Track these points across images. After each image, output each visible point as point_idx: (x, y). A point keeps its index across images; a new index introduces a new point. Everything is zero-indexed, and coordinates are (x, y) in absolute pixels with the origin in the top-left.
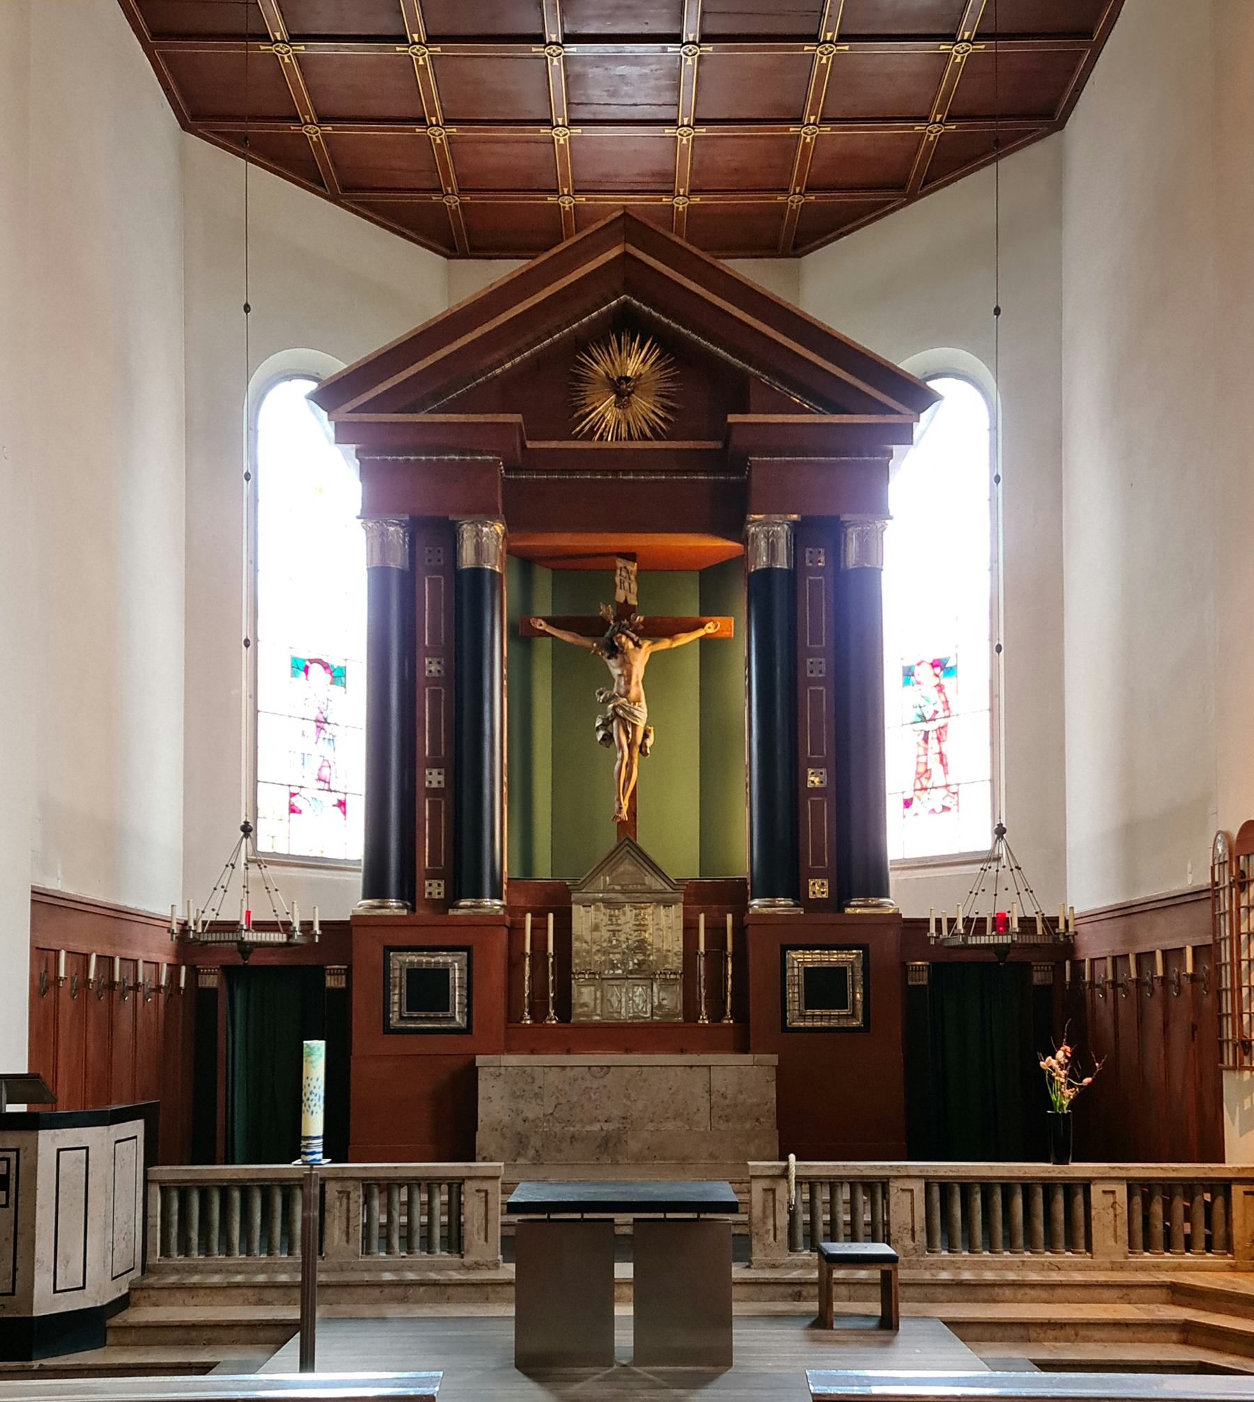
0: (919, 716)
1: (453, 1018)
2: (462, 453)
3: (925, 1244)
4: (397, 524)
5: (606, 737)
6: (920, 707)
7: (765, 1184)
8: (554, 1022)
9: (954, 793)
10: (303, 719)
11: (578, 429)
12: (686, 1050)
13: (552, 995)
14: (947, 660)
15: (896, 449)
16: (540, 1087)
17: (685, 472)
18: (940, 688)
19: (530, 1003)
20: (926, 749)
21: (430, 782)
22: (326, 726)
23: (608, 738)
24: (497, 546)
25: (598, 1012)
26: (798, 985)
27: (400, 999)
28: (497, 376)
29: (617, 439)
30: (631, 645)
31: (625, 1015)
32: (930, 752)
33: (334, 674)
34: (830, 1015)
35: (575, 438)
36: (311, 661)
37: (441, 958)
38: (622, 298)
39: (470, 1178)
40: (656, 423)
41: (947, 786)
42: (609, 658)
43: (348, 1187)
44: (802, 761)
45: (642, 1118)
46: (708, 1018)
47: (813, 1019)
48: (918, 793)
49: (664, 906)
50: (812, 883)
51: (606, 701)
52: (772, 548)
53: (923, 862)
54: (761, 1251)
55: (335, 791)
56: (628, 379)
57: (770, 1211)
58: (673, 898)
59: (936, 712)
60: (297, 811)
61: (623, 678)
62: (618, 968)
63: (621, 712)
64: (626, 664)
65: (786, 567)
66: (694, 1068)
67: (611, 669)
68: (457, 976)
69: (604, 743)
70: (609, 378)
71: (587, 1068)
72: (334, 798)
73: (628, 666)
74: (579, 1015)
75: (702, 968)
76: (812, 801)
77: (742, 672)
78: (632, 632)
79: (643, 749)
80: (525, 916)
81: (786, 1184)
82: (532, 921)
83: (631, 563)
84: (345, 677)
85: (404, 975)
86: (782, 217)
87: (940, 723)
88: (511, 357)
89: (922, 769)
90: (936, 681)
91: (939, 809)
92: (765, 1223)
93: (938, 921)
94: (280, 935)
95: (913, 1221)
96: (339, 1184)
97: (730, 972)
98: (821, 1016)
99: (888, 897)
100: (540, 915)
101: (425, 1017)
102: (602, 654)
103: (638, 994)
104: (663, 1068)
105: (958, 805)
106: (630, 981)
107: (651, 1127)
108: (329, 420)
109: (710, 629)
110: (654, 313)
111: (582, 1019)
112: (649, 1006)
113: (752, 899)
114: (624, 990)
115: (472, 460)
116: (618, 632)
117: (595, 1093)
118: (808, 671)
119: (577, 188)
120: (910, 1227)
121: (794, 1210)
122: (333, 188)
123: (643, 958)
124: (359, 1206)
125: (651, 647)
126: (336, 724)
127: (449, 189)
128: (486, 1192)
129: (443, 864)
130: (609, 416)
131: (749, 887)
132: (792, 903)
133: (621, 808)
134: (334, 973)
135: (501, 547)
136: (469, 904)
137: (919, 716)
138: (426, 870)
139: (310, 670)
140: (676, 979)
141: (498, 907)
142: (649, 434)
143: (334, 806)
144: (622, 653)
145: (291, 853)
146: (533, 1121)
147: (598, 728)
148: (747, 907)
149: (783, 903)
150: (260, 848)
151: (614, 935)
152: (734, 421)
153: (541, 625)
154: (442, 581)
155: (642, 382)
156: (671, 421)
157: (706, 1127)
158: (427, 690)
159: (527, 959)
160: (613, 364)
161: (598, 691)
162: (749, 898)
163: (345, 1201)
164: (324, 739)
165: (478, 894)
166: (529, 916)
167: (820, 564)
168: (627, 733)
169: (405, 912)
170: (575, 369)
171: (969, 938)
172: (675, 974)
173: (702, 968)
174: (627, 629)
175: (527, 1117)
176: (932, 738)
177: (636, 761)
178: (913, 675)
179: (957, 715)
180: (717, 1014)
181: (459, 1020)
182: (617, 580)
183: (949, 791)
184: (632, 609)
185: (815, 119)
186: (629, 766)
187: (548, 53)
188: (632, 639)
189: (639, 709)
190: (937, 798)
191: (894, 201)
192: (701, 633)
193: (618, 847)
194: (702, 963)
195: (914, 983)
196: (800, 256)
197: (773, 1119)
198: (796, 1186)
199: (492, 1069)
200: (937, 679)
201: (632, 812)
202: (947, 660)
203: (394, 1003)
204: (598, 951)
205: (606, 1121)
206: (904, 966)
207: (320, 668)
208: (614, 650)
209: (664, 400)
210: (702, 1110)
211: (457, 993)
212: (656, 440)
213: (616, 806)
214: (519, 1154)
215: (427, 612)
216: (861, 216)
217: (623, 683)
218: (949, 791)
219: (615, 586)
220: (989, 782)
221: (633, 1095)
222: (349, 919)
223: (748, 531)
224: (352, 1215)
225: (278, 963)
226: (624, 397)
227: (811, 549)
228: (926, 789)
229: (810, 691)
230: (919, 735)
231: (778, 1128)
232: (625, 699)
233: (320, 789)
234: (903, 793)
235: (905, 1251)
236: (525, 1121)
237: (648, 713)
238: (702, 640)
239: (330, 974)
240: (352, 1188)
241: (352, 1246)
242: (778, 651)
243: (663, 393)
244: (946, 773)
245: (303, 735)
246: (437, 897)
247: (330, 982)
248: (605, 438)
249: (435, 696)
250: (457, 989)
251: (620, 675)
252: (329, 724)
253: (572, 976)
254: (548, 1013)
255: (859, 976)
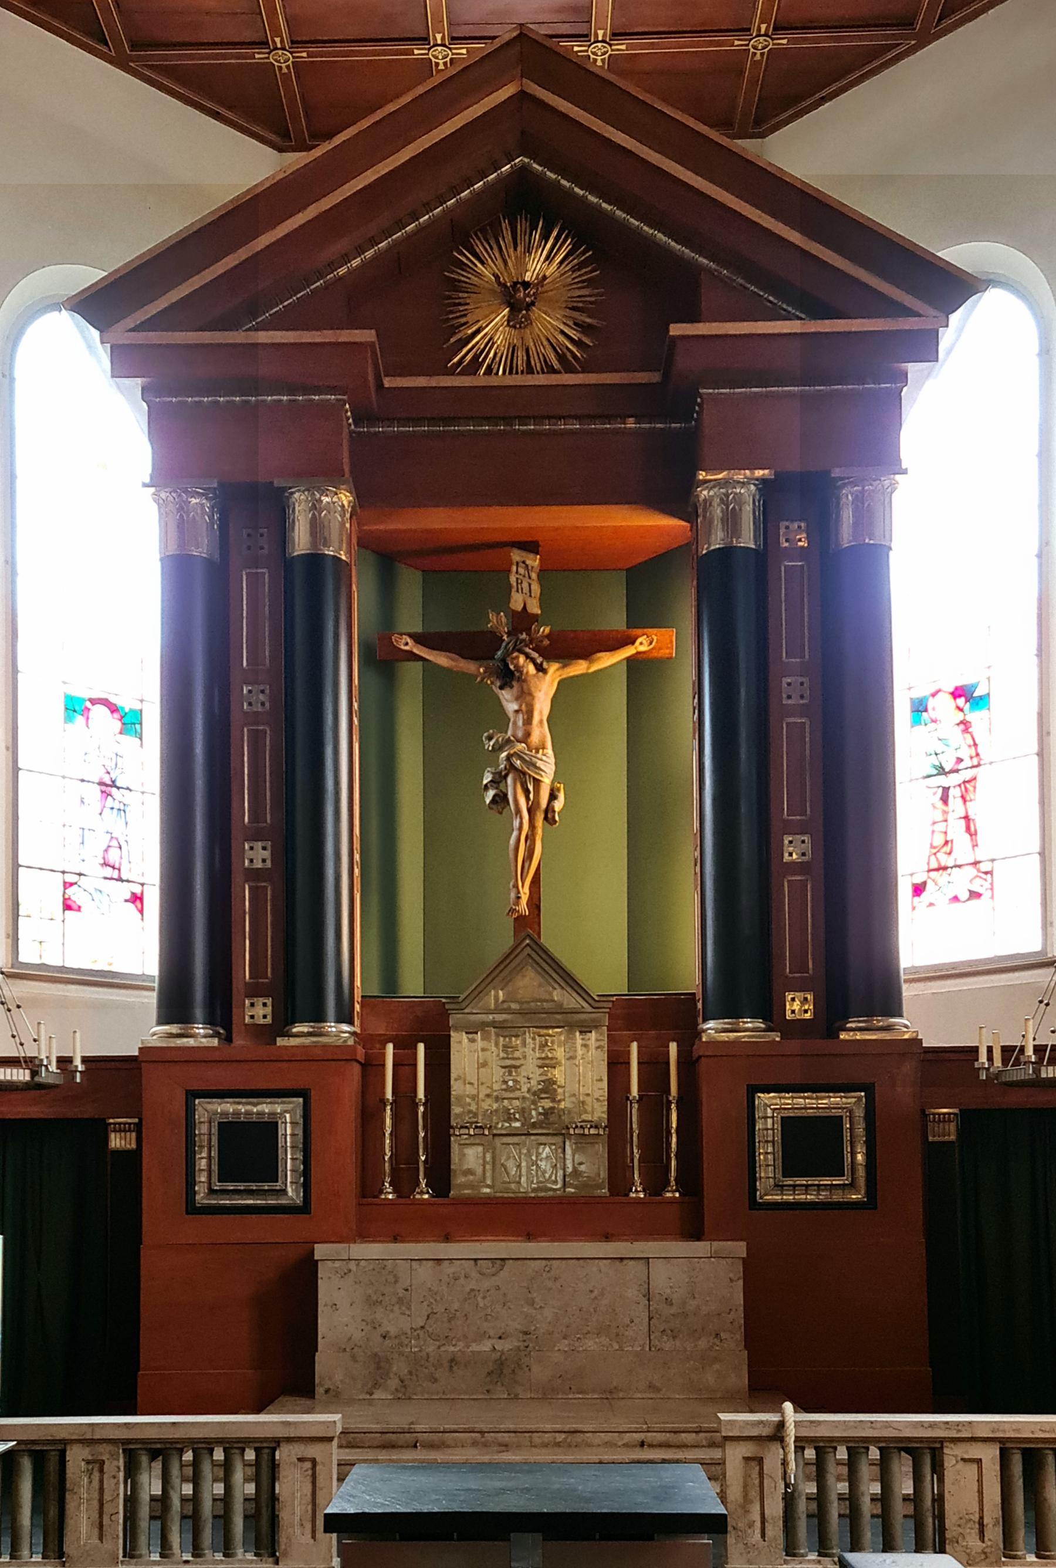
0: (935, 767)
1: (284, 1191)
2: (292, 390)
3: (1002, 1546)
4: (203, 494)
5: (497, 798)
6: (936, 754)
7: (746, 1449)
8: (426, 1196)
9: (986, 873)
10: (83, 781)
11: (455, 360)
12: (613, 1235)
13: (423, 1158)
14: (974, 687)
15: (913, 369)
16: (407, 1290)
17: (608, 418)
18: (965, 725)
19: (392, 1169)
20: (945, 813)
21: (251, 861)
22: (114, 790)
23: (501, 799)
24: (343, 524)
25: (489, 1182)
26: (773, 1142)
27: (209, 1165)
28: (341, 278)
29: (511, 373)
30: (531, 669)
31: (526, 1186)
32: (951, 817)
33: (125, 720)
34: (818, 1186)
35: (451, 372)
36: (93, 701)
37: (265, 1107)
38: (517, 161)
39: (289, 1440)
40: (567, 348)
41: (976, 863)
42: (501, 688)
43: (101, 1454)
44: (775, 826)
45: (551, 1333)
46: (644, 1190)
47: (794, 1191)
48: (933, 874)
49: (581, 1032)
50: (790, 997)
51: (498, 748)
52: (731, 521)
53: (941, 970)
54: (741, 1554)
55: (128, 881)
56: (526, 285)
57: (754, 1494)
58: (593, 1020)
59: (960, 760)
60: (74, 906)
61: (521, 716)
62: (517, 1120)
63: (518, 762)
64: (525, 697)
65: (753, 547)
66: (625, 1262)
67: (504, 703)
68: (289, 1132)
69: (494, 807)
70: (499, 283)
71: (472, 1262)
72: (126, 890)
73: (528, 698)
74: (461, 1185)
75: (634, 1119)
76: (789, 881)
77: (688, 701)
78: (533, 649)
79: (549, 816)
80: (384, 1048)
81: (781, 1451)
82: (394, 1053)
83: (532, 556)
84: (141, 724)
85: (215, 1130)
86: (741, 72)
87: (967, 775)
88: (360, 250)
89: (939, 840)
90: (960, 716)
91: (964, 895)
92: (747, 1512)
93: (990, 1050)
94: (21, 1071)
95: (981, 1510)
96: (88, 1449)
97: (674, 1125)
98: (807, 1186)
99: (901, 1016)
100: (407, 1046)
101: (245, 1190)
102: (492, 683)
103: (544, 1155)
104: (581, 1261)
105: (992, 889)
106: (533, 1138)
107: (564, 1345)
108: (102, 342)
109: (642, 645)
110: (564, 182)
111: (466, 1191)
112: (560, 1173)
113: (705, 1020)
114: (524, 1151)
115: (306, 400)
116: (514, 650)
117: (484, 1298)
118: (784, 696)
119: (454, 35)
120: (976, 1517)
121: (792, 1493)
122: (118, 45)
123: (551, 1105)
124: (118, 1483)
125: (558, 673)
126: (128, 789)
127: (278, 40)
128: (314, 1462)
129: (269, 974)
130: (499, 339)
131: (700, 1005)
132: (762, 1026)
133: (519, 898)
134: (121, 1129)
135: (348, 525)
136: (306, 1030)
137: (935, 767)
138: (246, 983)
139: (91, 714)
140: (598, 1135)
141: (346, 1035)
142: (556, 365)
143: (126, 901)
144: (519, 679)
145: (67, 965)
146: (396, 1337)
147: (486, 785)
148: (698, 1034)
149: (750, 1025)
150: (23, 958)
151: (510, 1074)
152: (678, 333)
153: (407, 644)
154: (267, 576)
155: (545, 288)
156: (589, 346)
157: (643, 1346)
158: (245, 730)
159: (389, 1107)
160: (505, 262)
161: (486, 734)
162: (700, 1020)
163: (96, 1476)
164: (112, 808)
165: (319, 1016)
166: (390, 1047)
167: (800, 544)
168: (527, 792)
169: (215, 1042)
170: (452, 272)
171: (1043, 1069)
172: (596, 1127)
173: (634, 1119)
174: (527, 646)
175: (388, 1332)
176: (954, 798)
177: (539, 832)
178: (926, 710)
179: (991, 763)
180: (656, 1185)
181: (293, 1194)
182: (513, 579)
183: (979, 871)
184: (535, 618)
185: (767, 29)
186: (530, 838)
187: (433, 56)
188: (533, 661)
189: (544, 758)
190: (961, 881)
191: (898, 45)
192: (629, 651)
193: (516, 947)
194: (634, 1111)
195: (936, 1139)
196: (762, 136)
197: (739, 1336)
198: (795, 1452)
199: (337, 1264)
200: (961, 714)
201: (535, 903)
202: (974, 687)
203: (201, 1170)
204: (488, 1096)
205: (500, 1338)
206: (924, 1115)
207: (105, 710)
208: (509, 677)
209: (576, 314)
210: (636, 1321)
211: (289, 1156)
212: (566, 373)
213: (513, 895)
214: (376, 1385)
215: (245, 621)
216: (849, 71)
217: (520, 723)
218: (979, 871)
219: (510, 587)
220: (1037, 857)
221: (539, 1302)
222: (136, 1054)
223: (698, 496)
224: (107, 1497)
225: (41, 1116)
226: (520, 311)
227: (787, 523)
228: (945, 868)
229: (788, 724)
230: (935, 794)
231: (746, 1347)
232: (523, 745)
233: (106, 878)
234: (912, 875)
235: (969, 1554)
236: (384, 1337)
237: (556, 764)
238: (632, 662)
239: (115, 1131)
240: (108, 1456)
241: (108, 1545)
242: (742, 666)
243: (575, 304)
244: (975, 845)
245: (83, 802)
246: (262, 1021)
247: (116, 1142)
248: (495, 371)
249: (256, 739)
250: (289, 1149)
251: (517, 712)
252: (118, 788)
253: (451, 1131)
254: (418, 1184)
255: (860, 1130)
